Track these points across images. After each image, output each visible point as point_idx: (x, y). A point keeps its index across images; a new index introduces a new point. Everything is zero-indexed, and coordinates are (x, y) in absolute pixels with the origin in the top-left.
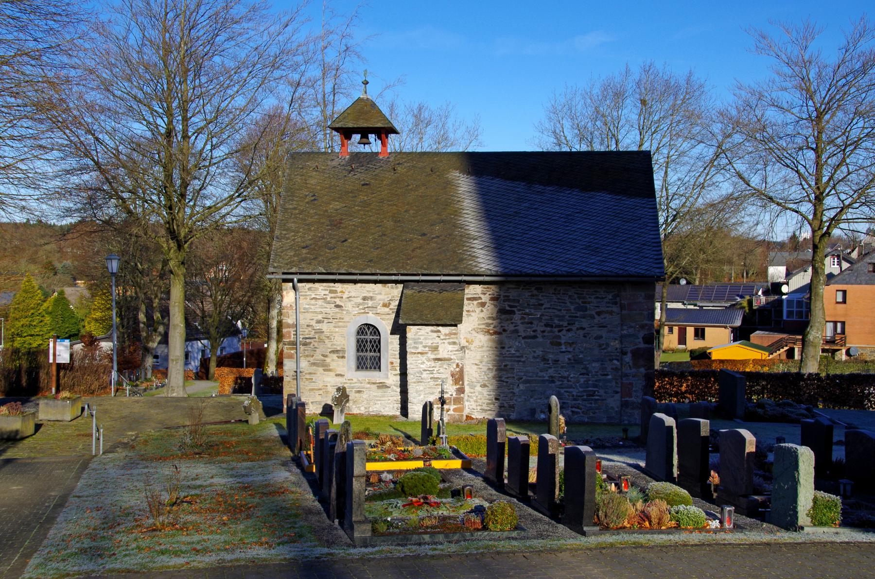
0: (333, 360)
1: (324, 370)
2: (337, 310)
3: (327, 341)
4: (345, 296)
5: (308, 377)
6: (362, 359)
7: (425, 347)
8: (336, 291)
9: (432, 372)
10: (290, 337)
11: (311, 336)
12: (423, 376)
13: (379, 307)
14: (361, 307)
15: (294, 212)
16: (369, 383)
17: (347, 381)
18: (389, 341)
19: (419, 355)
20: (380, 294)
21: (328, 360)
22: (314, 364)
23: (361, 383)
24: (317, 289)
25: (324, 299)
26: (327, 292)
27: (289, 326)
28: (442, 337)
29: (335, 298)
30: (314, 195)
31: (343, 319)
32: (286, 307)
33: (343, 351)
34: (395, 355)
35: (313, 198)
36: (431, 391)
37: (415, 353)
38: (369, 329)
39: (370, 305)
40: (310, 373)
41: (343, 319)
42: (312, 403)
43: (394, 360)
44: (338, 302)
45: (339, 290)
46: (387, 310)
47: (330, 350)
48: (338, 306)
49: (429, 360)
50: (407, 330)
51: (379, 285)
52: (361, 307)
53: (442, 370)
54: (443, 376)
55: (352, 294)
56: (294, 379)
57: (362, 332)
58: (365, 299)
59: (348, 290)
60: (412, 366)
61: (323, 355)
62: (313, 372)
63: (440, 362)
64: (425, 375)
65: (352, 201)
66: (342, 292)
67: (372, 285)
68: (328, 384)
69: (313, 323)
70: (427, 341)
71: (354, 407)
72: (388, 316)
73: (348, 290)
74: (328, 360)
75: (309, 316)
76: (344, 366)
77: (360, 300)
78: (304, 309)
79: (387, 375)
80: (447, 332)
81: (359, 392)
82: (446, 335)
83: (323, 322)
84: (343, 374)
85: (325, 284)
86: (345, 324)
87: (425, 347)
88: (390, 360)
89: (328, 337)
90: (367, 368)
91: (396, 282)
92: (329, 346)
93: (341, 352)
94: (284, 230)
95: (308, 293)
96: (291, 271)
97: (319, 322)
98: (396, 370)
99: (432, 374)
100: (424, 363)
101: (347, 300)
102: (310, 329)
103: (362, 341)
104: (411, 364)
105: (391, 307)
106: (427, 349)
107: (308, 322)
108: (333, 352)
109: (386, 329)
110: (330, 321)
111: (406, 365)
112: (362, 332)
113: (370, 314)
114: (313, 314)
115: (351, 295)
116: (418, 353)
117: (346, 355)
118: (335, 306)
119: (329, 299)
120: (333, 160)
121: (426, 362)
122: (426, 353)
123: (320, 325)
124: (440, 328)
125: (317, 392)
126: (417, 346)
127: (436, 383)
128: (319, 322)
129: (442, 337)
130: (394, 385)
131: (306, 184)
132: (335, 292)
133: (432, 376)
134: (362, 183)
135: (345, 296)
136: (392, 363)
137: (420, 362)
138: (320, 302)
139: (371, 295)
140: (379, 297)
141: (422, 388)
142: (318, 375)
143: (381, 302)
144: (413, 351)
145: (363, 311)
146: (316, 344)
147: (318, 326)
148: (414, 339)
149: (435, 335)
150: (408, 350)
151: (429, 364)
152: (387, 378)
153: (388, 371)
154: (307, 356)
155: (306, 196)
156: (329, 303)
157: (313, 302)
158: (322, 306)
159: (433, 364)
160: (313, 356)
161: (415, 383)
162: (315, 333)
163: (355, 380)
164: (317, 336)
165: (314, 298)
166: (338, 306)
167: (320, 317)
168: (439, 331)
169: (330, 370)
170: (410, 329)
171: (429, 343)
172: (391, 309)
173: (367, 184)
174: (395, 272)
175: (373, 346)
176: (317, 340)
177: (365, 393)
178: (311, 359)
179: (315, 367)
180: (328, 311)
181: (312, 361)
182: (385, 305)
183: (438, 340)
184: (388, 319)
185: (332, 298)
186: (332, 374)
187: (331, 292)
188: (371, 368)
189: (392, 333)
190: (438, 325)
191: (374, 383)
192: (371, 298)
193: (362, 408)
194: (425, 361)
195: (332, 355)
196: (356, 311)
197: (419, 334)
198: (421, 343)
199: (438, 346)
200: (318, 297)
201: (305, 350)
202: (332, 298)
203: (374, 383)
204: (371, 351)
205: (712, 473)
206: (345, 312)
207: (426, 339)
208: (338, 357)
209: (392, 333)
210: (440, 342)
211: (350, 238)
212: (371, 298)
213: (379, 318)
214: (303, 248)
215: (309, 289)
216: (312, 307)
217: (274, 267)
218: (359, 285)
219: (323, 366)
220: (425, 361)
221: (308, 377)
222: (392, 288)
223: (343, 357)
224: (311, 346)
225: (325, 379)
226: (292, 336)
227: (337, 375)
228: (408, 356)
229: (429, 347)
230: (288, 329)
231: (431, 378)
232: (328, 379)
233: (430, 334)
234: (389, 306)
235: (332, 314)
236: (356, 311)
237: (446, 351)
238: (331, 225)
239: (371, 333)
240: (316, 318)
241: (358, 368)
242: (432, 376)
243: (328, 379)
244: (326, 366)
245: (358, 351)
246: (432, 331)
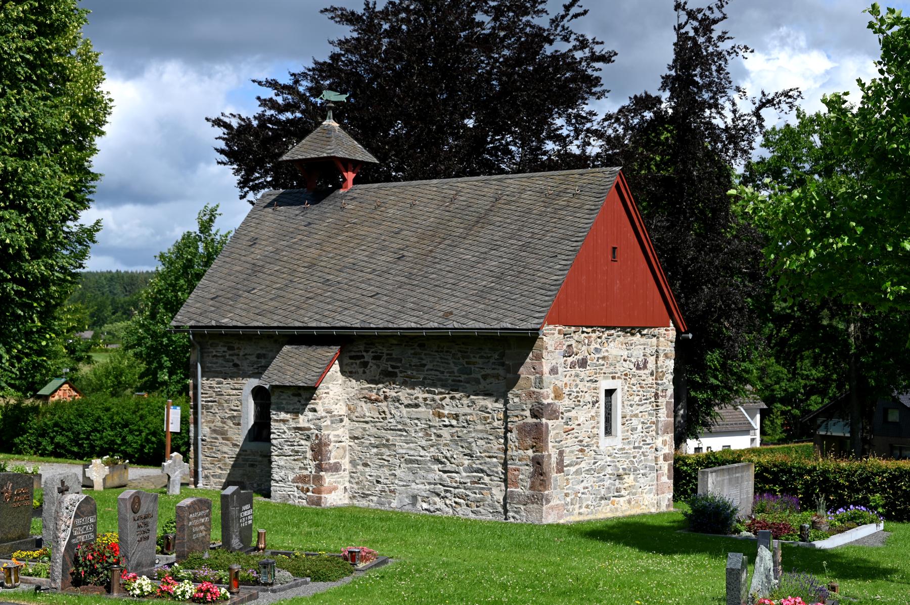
26: (225, 349)
27: (666, 356)
119: (228, 357)
145: (256, 371)
149: (296, 399)
178: (212, 425)
194: (287, 431)
216: (214, 366)
223: (239, 424)
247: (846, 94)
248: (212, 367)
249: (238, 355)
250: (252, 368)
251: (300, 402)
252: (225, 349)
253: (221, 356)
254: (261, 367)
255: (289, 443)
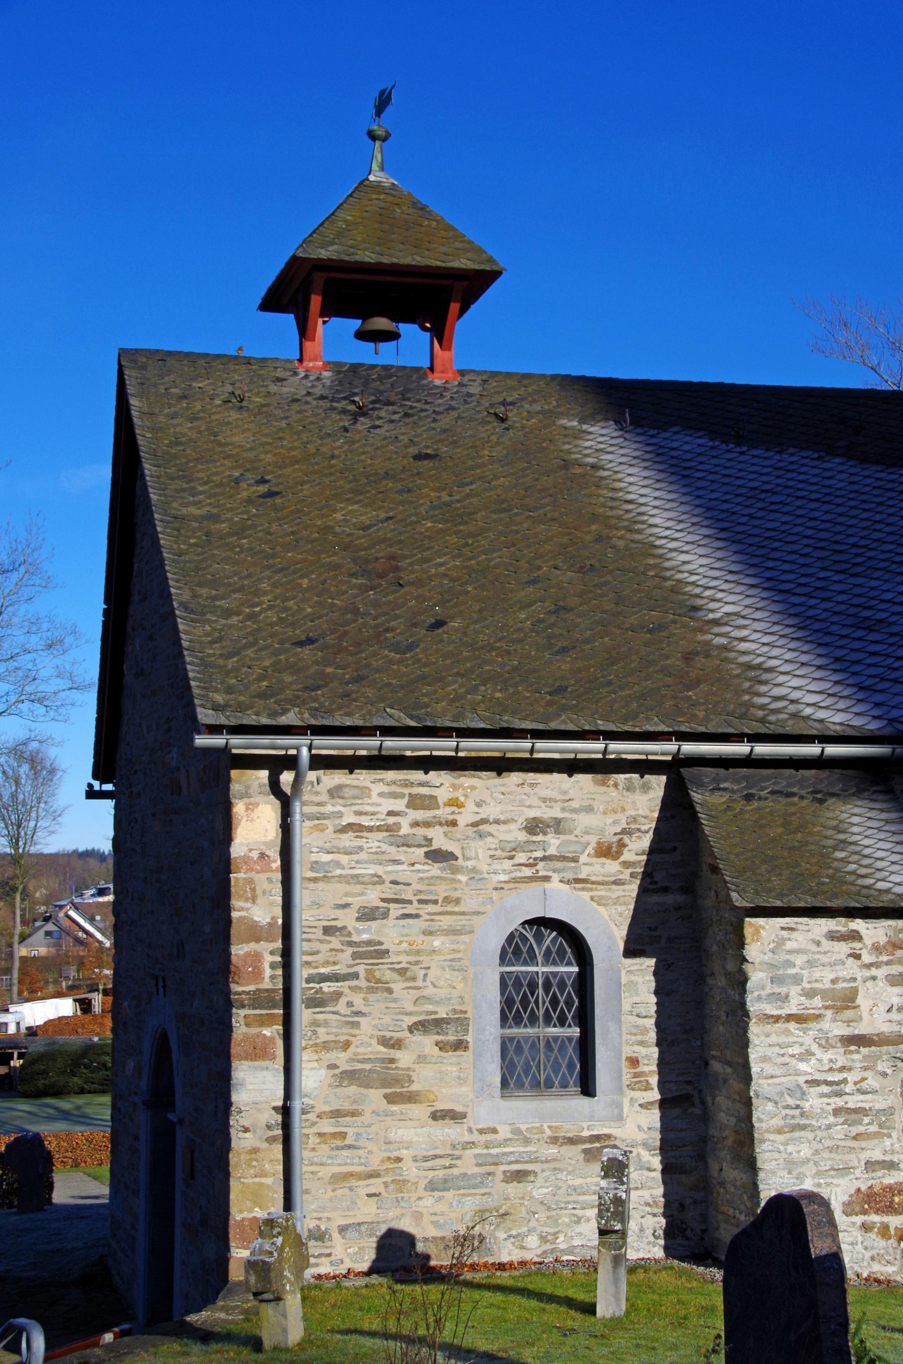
0: (422, 1059)
1: (390, 1099)
2: (435, 870)
3: (398, 986)
4: (465, 817)
5: (327, 1126)
6: (519, 1049)
7: (810, 994)
8: (433, 798)
9: (837, 1089)
10: (257, 974)
11: (340, 969)
12: (806, 1105)
13: (583, 859)
14: (521, 858)
15: (215, 527)
16: (554, 1140)
17: (476, 1137)
18: (624, 980)
19: (792, 1026)
20: (589, 809)
21: (405, 1059)
22: (350, 1076)
23: (527, 1141)
24: (364, 792)
25: (388, 828)
26: (399, 805)
27: (255, 933)
28: (867, 958)
29: (427, 824)
30: (263, 481)
31: (457, 901)
32: (246, 859)
33: (460, 1021)
34: (645, 1031)
35: (263, 489)
36: (838, 1160)
37: (777, 1019)
38: (539, 938)
39: (552, 851)
40: (336, 1114)
41: (457, 901)
42: (342, 1229)
43: (641, 1051)
44: (440, 840)
45: (443, 795)
46: (612, 867)
47: (410, 1020)
48: (437, 856)
49: (826, 1044)
50: (748, 931)
51: (584, 780)
52: (521, 858)
53: (872, 1082)
54: (879, 1103)
55: (491, 811)
56: (271, 1140)
57: (517, 952)
58: (534, 827)
59: (475, 796)
60: (769, 1069)
61: (384, 1042)
62: (346, 1106)
63: (864, 1051)
64: (814, 1101)
65: (402, 503)
66: (454, 803)
67: (558, 779)
68: (404, 1153)
69: (348, 919)
70: (817, 974)
71: (502, 1235)
72: (618, 892)
73: (475, 796)
74: (405, 1059)
75: (332, 892)
76: (462, 1082)
77: (515, 834)
78: (315, 866)
79: (620, 1106)
80: (883, 940)
81: (519, 1176)
82: (877, 949)
83: (385, 915)
84: (459, 1108)
85: (390, 775)
86: (461, 921)
87: (810, 994)
88: (627, 1051)
89: (402, 972)
90: (536, 1085)
91: (644, 767)
92: (410, 1007)
93: (451, 1028)
94: (201, 585)
95: (329, 808)
96: (284, 720)
97: (368, 915)
98: (647, 1087)
99: (840, 1094)
100: (810, 1053)
101: (470, 831)
102: (335, 942)
103: (518, 983)
104: (765, 1059)
105: (627, 856)
106: (817, 1002)
107: (327, 915)
108: (421, 1027)
109: (611, 937)
110: (410, 910)
111: (285, 1089)
112: (517, 952)
113: (555, 885)
114: (343, 887)
115: (484, 813)
116: (789, 1018)
117: (469, 1038)
118: (427, 855)
119: (405, 830)
120: (279, 380)
121: (819, 1053)
122: (818, 1017)
123: (374, 925)
124: (858, 924)
125: (364, 1187)
126: (783, 990)
127: (854, 1130)
128: (368, 915)
129: (867, 958)
130: (645, 1145)
131: (220, 444)
132: (429, 802)
133: (839, 1102)
134: (413, 450)
135: (465, 817)
136: (634, 1062)
137: (796, 1050)
138: (374, 842)
139: (556, 813)
140: (584, 820)
141: (805, 1151)
142: (367, 1118)
143: (593, 840)
144: (770, 1010)
145: (527, 872)
146: (358, 1000)
147: (365, 932)
148: (772, 966)
149: (843, 948)
150: (753, 1006)
151: (826, 1056)
152: (620, 1118)
153: (620, 1091)
154: (326, 1046)
155: (237, 481)
156: (406, 843)
157: (347, 841)
158: (379, 858)
159: (839, 1056)
160: (346, 1045)
161: (780, 1131)
162: (355, 956)
163: (504, 1132)
164: (361, 969)
165: (350, 827)
166: (437, 856)
167: (373, 897)
168: (855, 936)
169: (411, 1098)
170: (757, 931)
171: (825, 977)
172: (626, 864)
173: (427, 456)
174: (662, 728)
175: (555, 1002)
176: (362, 983)
177: (540, 1181)
178: (342, 1059)
179: (353, 1090)
180: (402, 872)
181: (345, 1067)
182: (605, 851)
183: (852, 968)
184: (617, 901)
185: (415, 824)
186: (420, 1111)
187: (415, 802)
188: (549, 1084)
189: (631, 951)
190: (851, 913)
191: (572, 1141)
192: (557, 826)
193: (532, 1241)
194: (814, 1048)
195: (418, 1038)
196: (503, 870)
197: (789, 945)
198: (797, 980)
199: (855, 992)
200: (365, 821)
201: (315, 1023)
202: (415, 824)
203: (572, 1141)
204: (548, 1020)
205: (188, 1319)
206: (463, 878)
207: (811, 964)
208: (442, 1046)
209: (631, 951)
210: (860, 974)
211: (452, 618)
212: (557, 826)
213: (586, 895)
214: (301, 644)
215: (335, 792)
216: (344, 859)
217: (216, 708)
218: (515, 778)
219: (385, 1084)
220: (814, 1048)
221: (327, 1126)
222: (629, 788)
223: (460, 1045)
224: (341, 1007)
225: (392, 1136)
226: (268, 972)
227: (436, 1116)
228: (755, 1030)
229: (824, 993)
230: (252, 946)
231: (837, 1112)
232: (402, 1133)
233: (826, 944)
234: (619, 853)
235: (416, 886)
236: (503, 870)
237: (883, 1008)
238: (365, 573)
239: (548, 953)
240: (357, 902)
241: (504, 1084)
242: (839, 1102)
243: (402, 1133)
244: (397, 1081)
245: (504, 1018)
246: (833, 936)
247: (240, 349)
248: (338, 864)
249: (454, 823)
250: (507, 864)
251: (858, 957)
252: (399, 805)
253: (379, 829)
254: (544, 859)
255: (825, 1089)
